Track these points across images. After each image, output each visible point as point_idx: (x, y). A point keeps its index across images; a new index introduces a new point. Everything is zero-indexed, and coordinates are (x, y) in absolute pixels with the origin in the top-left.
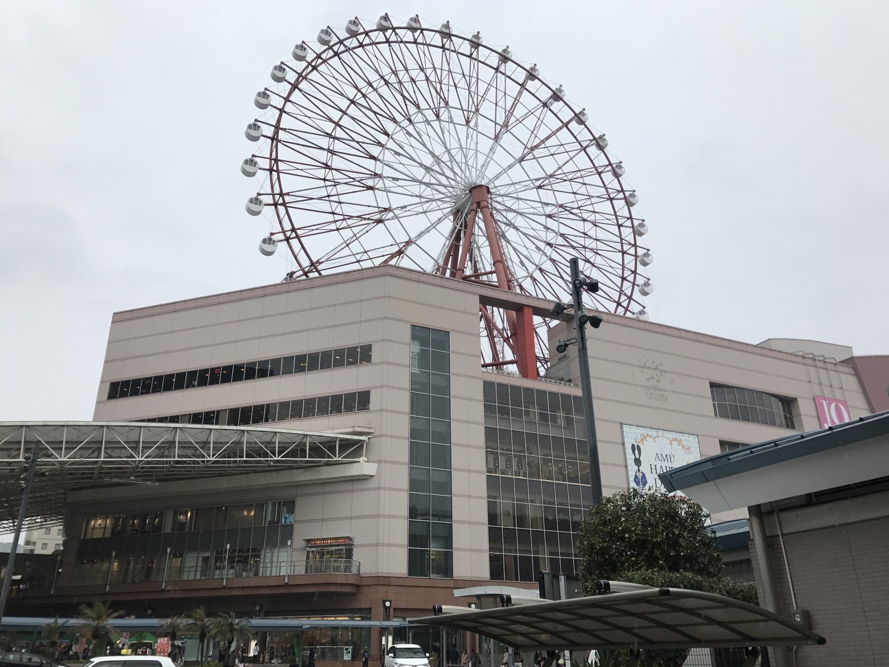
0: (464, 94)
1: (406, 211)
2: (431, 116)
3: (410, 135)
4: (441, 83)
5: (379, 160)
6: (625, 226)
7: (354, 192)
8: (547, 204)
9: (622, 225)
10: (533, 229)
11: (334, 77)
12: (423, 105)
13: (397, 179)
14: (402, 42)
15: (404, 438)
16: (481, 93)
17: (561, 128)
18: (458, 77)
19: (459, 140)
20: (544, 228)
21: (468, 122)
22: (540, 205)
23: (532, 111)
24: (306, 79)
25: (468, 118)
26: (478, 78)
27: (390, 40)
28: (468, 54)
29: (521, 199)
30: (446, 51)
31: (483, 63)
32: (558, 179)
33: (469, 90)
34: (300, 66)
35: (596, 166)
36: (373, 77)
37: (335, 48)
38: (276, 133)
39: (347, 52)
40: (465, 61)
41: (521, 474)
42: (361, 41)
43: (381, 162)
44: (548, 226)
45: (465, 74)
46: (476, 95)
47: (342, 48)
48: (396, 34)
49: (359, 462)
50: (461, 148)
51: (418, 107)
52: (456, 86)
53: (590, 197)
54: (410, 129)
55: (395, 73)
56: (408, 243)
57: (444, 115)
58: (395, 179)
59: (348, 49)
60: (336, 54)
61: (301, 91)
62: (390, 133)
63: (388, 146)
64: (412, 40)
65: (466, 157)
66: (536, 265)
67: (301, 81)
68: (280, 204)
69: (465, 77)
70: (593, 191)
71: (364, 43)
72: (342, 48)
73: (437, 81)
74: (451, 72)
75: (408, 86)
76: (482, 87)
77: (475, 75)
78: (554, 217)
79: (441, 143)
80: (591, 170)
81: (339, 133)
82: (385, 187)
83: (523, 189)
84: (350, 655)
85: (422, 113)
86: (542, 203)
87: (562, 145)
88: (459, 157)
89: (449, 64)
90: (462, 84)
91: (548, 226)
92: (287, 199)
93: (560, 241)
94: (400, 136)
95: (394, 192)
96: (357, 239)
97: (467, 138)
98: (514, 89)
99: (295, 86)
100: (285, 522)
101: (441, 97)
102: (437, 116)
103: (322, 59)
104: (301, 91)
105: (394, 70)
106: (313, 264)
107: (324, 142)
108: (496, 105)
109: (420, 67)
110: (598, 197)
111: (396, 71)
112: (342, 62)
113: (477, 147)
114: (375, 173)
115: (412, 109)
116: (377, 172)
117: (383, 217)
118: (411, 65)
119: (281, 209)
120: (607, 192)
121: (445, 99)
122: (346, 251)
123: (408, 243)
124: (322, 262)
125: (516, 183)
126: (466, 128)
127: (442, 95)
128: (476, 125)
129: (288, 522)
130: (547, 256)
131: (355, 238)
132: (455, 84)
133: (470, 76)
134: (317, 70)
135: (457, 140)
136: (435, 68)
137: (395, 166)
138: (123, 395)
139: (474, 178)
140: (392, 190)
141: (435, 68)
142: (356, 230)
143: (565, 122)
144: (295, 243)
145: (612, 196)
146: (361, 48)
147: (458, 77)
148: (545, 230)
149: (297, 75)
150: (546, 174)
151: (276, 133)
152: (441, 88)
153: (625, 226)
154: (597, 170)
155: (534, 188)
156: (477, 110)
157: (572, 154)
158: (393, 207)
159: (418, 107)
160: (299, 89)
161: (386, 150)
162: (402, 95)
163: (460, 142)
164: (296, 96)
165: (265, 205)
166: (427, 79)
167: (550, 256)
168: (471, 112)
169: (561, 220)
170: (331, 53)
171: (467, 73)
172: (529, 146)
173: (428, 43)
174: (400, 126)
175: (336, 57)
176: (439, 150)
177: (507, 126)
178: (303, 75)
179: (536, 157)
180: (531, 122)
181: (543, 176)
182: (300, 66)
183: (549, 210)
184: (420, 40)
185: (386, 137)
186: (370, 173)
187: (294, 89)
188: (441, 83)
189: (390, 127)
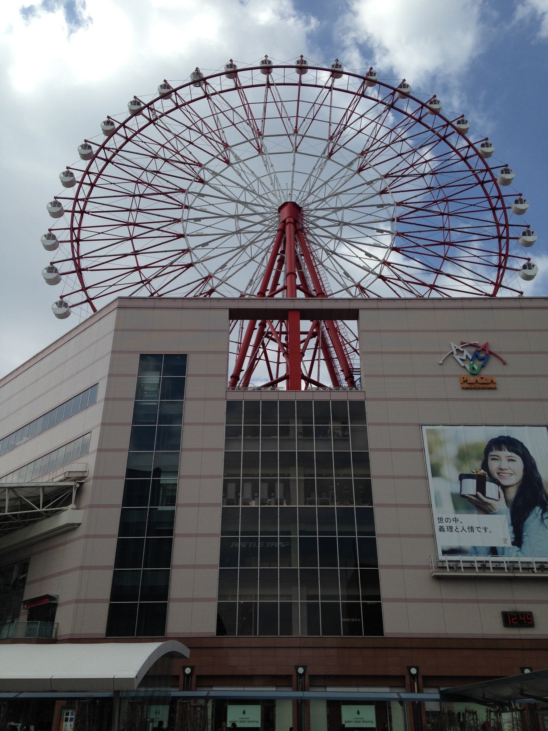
0: (202, 142)
1: (254, 283)
2: (197, 187)
3: (199, 219)
4: (178, 153)
5: (196, 263)
6: (423, 117)
8: (351, 163)
10: (359, 194)
11: (99, 233)
12: (184, 185)
13: (206, 244)
14: (117, 151)
16: (214, 128)
18: (186, 135)
19: (238, 184)
20: (368, 185)
21: (227, 162)
22: (346, 170)
24: (81, 257)
25: (224, 158)
26: (201, 119)
27: (108, 158)
30: (156, 122)
31: (192, 101)
32: (374, 150)
33: (203, 135)
34: (65, 221)
35: (356, 92)
36: (127, 202)
37: (77, 209)
39: (88, 203)
40: (177, 114)
42: (89, 182)
43: (199, 263)
44: (368, 180)
45: (189, 126)
46: (212, 133)
48: (108, 149)
50: (245, 189)
51: (182, 191)
52: (191, 143)
54: (193, 214)
55: (138, 182)
57: (206, 176)
58: (204, 245)
59: (86, 200)
60: (82, 212)
62: (182, 233)
63: (192, 246)
64: (124, 140)
65: (253, 191)
66: (388, 220)
67: (79, 262)
69: (191, 129)
71: (93, 182)
72: (82, 203)
73: (174, 153)
74: (178, 136)
75: (156, 181)
76: (210, 122)
77: (196, 119)
78: (364, 166)
79: (226, 201)
81: (147, 273)
82: (220, 280)
83: (320, 170)
85: (190, 193)
86: (345, 167)
87: (363, 116)
88: (249, 198)
89: (169, 131)
90: (194, 136)
91: (368, 180)
93: (389, 181)
94: (191, 228)
95: (231, 276)
97: (240, 175)
98: (234, 98)
99: (79, 271)
101: (189, 164)
102: (201, 181)
103: (76, 228)
105: (136, 180)
107: (127, 247)
108: (234, 125)
109: (151, 157)
111: (139, 179)
112: (92, 213)
113: (255, 176)
114: (204, 278)
115: (180, 197)
116: (205, 276)
118: (144, 162)
120: (434, 132)
121: (194, 162)
125: (328, 181)
126: (357, 281)
127: (189, 162)
128: (236, 157)
130: (392, 205)
132: (188, 141)
133: (194, 124)
134: (81, 240)
135: (235, 185)
136: (163, 146)
137: (211, 255)
139: (277, 201)
140: (228, 275)
141: (163, 146)
146: (95, 188)
147: (186, 135)
148: (369, 186)
149: (69, 230)
150: (357, 154)
152: (182, 156)
153: (423, 117)
155: (355, 174)
156: (226, 146)
159: (182, 191)
160: (84, 270)
161: (194, 251)
162: (162, 193)
163: (240, 186)
164: (89, 278)
166: (166, 160)
167: (394, 202)
168: (222, 152)
169: (373, 163)
170: (78, 216)
171: (189, 124)
172: (291, 132)
173: (137, 130)
174: (185, 221)
175: (84, 214)
176: (231, 208)
177: (260, 134)
178: (76, 256)
179: (303, 134)
180: (272, 110)
181: (354, 158)
182: (65, 221)
184: (129, 134)
185: (182, 238)
186: (201, 281)
187: (81, 274)
188: (178, 153)
189: (178, 228)
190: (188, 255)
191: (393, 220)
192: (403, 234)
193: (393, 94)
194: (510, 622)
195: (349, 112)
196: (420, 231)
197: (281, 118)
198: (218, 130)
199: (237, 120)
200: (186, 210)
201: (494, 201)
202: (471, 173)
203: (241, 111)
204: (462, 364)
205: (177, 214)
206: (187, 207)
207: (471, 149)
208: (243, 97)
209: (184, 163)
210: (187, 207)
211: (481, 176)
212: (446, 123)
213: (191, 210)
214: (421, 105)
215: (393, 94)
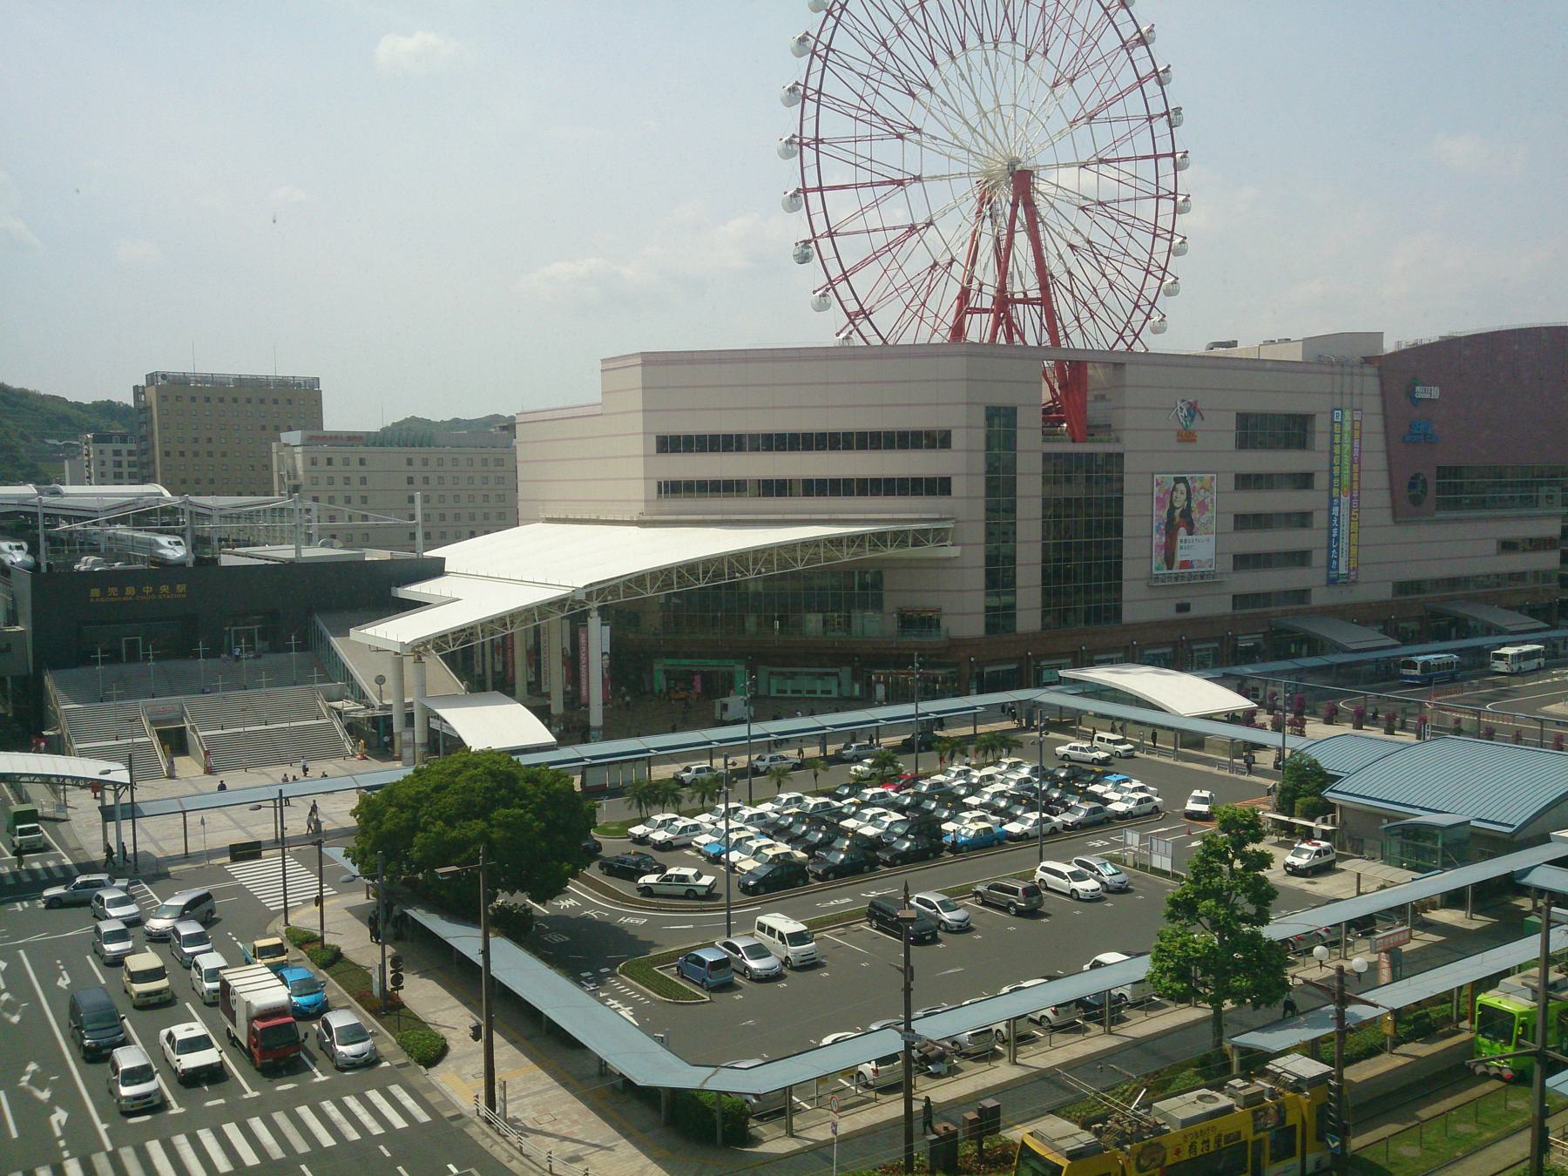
0: (1071, 50)
3: (987, 64)
12: (1020, 38)
18: (1076, 28)
21: (1056, 84)
29: (1054, 208)
31: (1115, 27)
53: (1127, 254)
68: (820, 57)
70: (1133, 249)
80: (1148, 225)
89: (1076, 7)
90: (1077, 38)
101: (1044, 39)
119: (818, 64)
122: (850, 146)
147: (1076, 28)
156: (1072, 80)
177: (1091, 118)
190: (947, 57)
193: (1171, 193)
194: (162, 984)
195: (1131, 221)
199: (1103, 87)
202: (1126, 320)
203: (1114, 91)
205: (987, 37)
206: (996, 46)
208: (1130, 90)
209: (1044, 33)
210: (996, 46)
211: (1127, 332)
215: (1171, 193)
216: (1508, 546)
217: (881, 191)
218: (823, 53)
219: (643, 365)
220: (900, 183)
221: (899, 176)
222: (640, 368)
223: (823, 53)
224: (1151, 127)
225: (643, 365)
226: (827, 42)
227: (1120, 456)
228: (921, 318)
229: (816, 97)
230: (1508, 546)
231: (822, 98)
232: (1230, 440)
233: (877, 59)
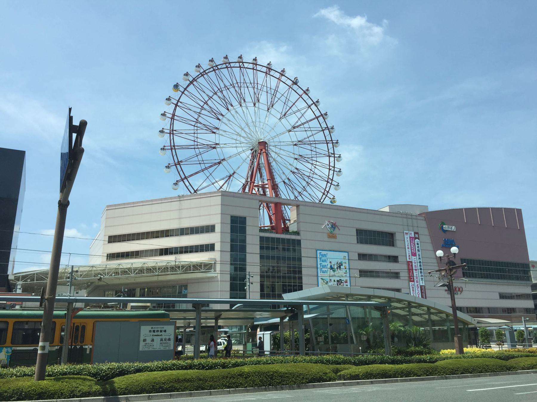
7: (206, 133)
9: (333, 167)
15: (228, 242)
17: (314, 119)
21: (255, 104)
23: (300, 110)
24: (196, 81)
28: (278, 78)
38: (177, 103)
41: (274, 272)
47: (216, 68)
49: (321, 272)
52: (248, 87)
56: (224, 160)
61: (194, 85)
67: (194, 81)
68: (330, 179)
84: (166, 327)
92: (174, 132)
96: (201, 154)
100: (184, 293)
103: (206, 72)
104: (194, 85)
106: (178, 162)
108: (267, 92)
110: (324, 154)
115: (242, 101)
117: (217, 146)
122: (196, 159)
123: (224, 160)
124: (183, 162)
129: (185, 293)
131: (200, 154)
132: (251, 84)
138: (114, 242)
142: (201, 150)
143: (317, 116)
144: (174, 150)
145: (330, 155)
151: (177, 103)
154: (327, 142)
157: (314, 132)
158: (220, 143)
165: (166, 133)
175: (214, 71)
183: (296, 157)
184: (255, 68)
191: (291, 171)
192: (290, 180)
195: (314, 143)
196: (233, 198)
197: (285, 103)
198: (260, 90)
200: (239, 106)
201: (326, 192)
203: (288, 108)
204: (328, 229)
207: (330, 168)
212: (333, 153)
213: (229, 113)
214: (331, 140)
215: (326, 128)
216: (503, 296)
217: (299, 123)
218: (329, 180)
219: (221, 195)
220: (294, 128)
221: (295, 130)
222: (220, 196)
223: (329, 180)
224: (293, 89)
225: (221, 195)
226: (328, 183)
227: (299, 242)
228: (251, 83)
229: (331, 168)
230: (503, 296)
231: (326, 142)
232: (354, 239)
233: (312, 171)
